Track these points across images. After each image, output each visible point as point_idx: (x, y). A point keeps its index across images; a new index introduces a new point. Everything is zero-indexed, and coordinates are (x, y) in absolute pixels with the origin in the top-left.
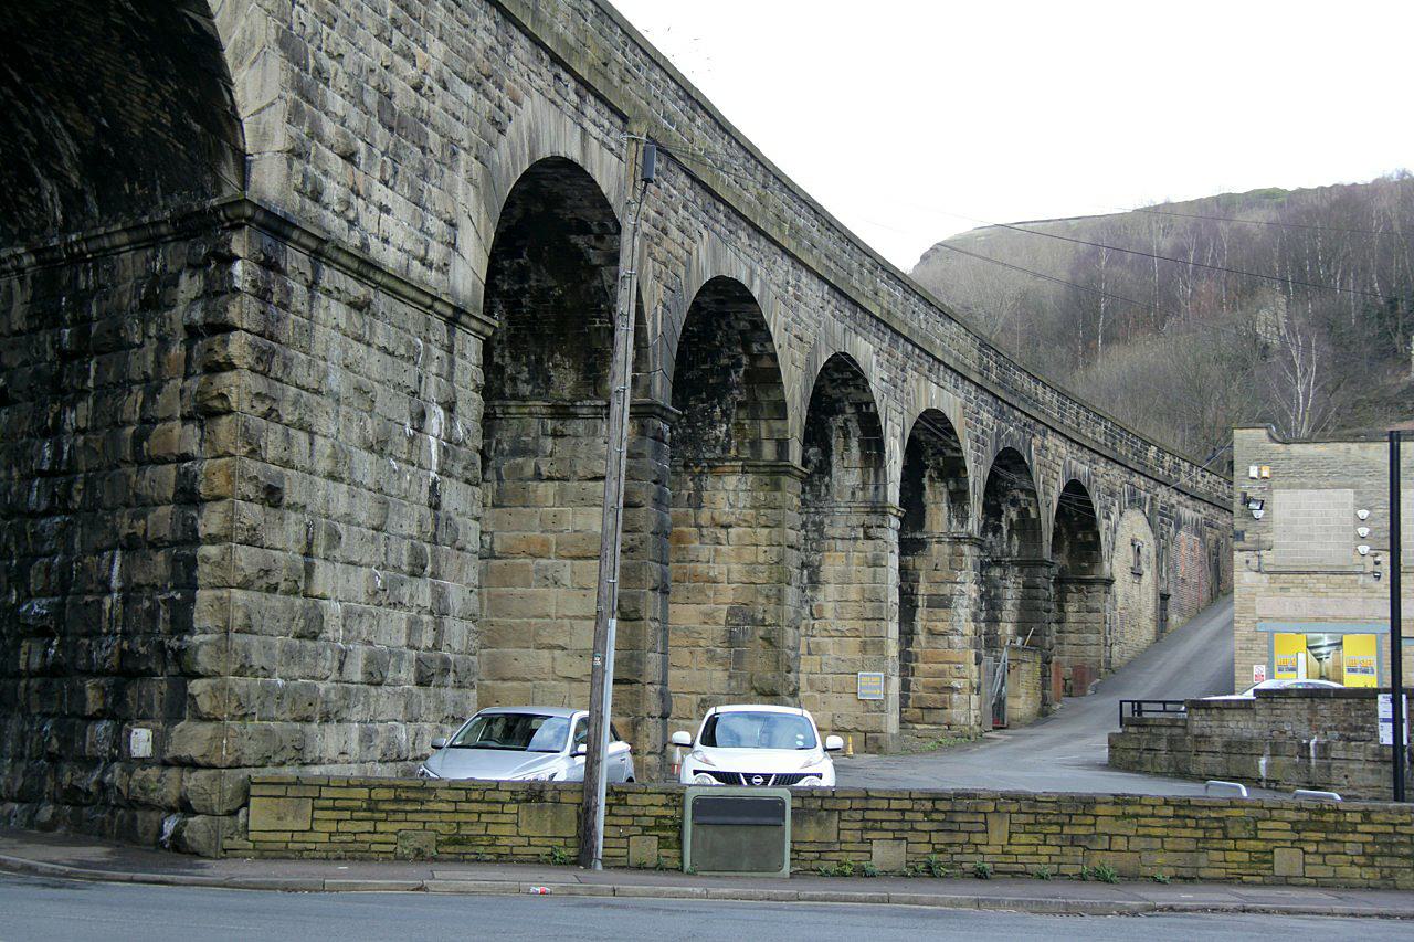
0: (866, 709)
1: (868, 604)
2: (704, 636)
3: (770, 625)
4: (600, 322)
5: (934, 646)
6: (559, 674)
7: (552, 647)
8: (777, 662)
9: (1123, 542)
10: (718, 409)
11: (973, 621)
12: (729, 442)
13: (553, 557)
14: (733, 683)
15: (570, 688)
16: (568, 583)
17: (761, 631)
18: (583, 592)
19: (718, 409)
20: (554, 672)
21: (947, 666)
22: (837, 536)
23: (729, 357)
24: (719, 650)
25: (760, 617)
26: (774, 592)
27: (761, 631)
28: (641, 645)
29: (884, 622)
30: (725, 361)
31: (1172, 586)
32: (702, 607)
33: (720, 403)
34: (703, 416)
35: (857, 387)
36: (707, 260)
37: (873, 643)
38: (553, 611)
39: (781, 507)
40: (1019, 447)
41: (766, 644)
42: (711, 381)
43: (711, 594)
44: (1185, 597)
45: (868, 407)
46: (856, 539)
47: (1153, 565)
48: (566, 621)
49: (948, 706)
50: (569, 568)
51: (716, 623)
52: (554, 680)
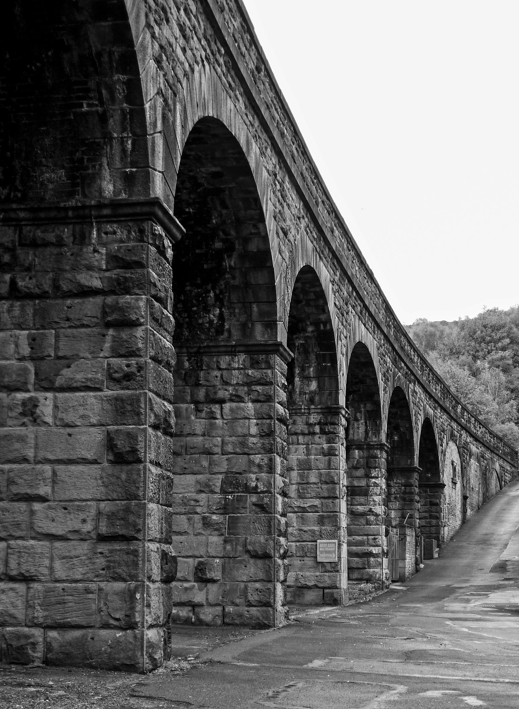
0: (323, 569)
1: (324, 486)
2: (201, 503)
3: (262, 492)
4: (89, 105)
5: (356, 523)
6: (40, 530)
7: (29, 499)
8: (270, 527)
9: (448, 462)
10: (212, 294)
11: (384, 505)
12: (223, 325)
13: (30, 387)
14: (228, 547)
15: (52, 548)
16: (49, 420)
17: (254, 499)
18: (69, 430)
19: (212, 294)
20: (32, 528)
21: (365, 537)
22: (299, 431)
23: (222, 241)
24: (214, 517)
25: (253, 484)
26: (266, 461)
27: (254, 499)
28: (141, 494)
29: (338, 500)
30: (218, 245)
31: (468, 492)
32: (199, 477)
33: (214, 288)
34: (198, 301)
35: (317, 307)
36: (209, 90)
37: (329, 517)
38: (30, 453)
39: (271, 383)
40: (404, 387)
41: (258, 510)
42: (205, 266)
43: (205, 464)
44: (475, 498)
45: (325, 326)
46: (314, 434)
47: (460, 478)
48: (47, 468)
49: (367, 567)
50: (50, 403)
51: (213, 492)
52: (33, 538)
